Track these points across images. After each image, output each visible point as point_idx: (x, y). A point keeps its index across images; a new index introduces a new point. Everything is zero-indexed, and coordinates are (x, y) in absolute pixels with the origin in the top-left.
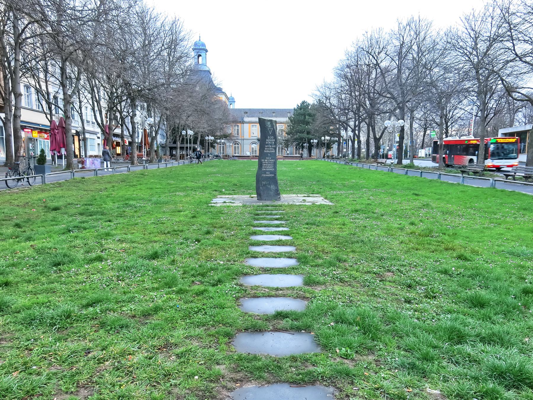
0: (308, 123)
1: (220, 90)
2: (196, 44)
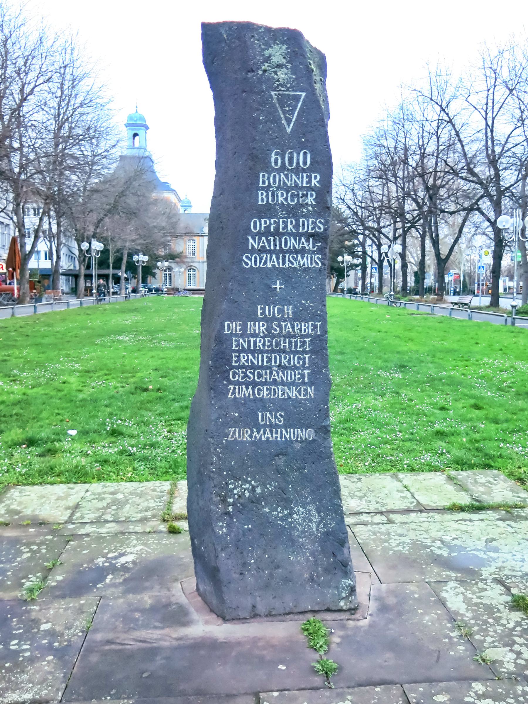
1: (166, 186)
2: (130, 118)
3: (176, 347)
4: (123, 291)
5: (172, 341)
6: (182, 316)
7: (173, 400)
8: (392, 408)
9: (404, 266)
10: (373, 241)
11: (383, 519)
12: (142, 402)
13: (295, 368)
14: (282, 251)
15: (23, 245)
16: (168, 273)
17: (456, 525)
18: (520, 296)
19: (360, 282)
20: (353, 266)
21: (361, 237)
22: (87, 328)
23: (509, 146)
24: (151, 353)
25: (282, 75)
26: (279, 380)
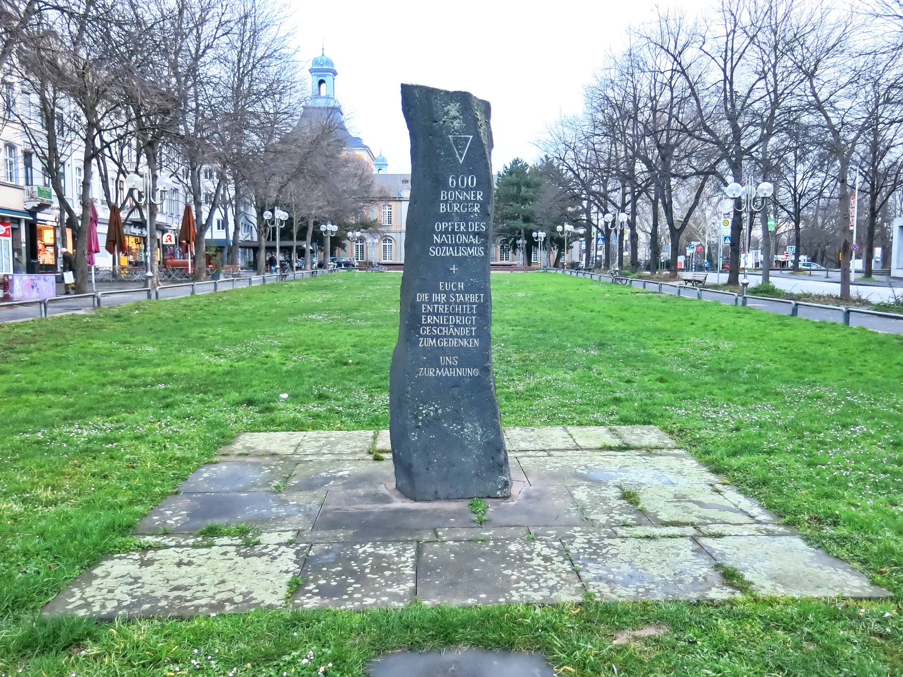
0: (525, 200)
1: (357, 142)
2: (316, 62)
3: (373, 326)
4: (308, 266)
5: (367, 319)
6: (377, 294)
7: (373, 372)
8: (580, 382)
9: (634, 237)
10: (599, 208)
11: (546, 454)
12: (343, 373)
13: (465, 326)
14: (456, 244)
15: (199, 214)
16: (359, 244)
17: (602, 458)
18: (761, 272)
19: (584, 256)
20: (576, 237)
21: (585, 203)
22: (276, 307)
23: (749, 101)
24: (347, 332)
25: (456, 124)
26: (454, 334)
